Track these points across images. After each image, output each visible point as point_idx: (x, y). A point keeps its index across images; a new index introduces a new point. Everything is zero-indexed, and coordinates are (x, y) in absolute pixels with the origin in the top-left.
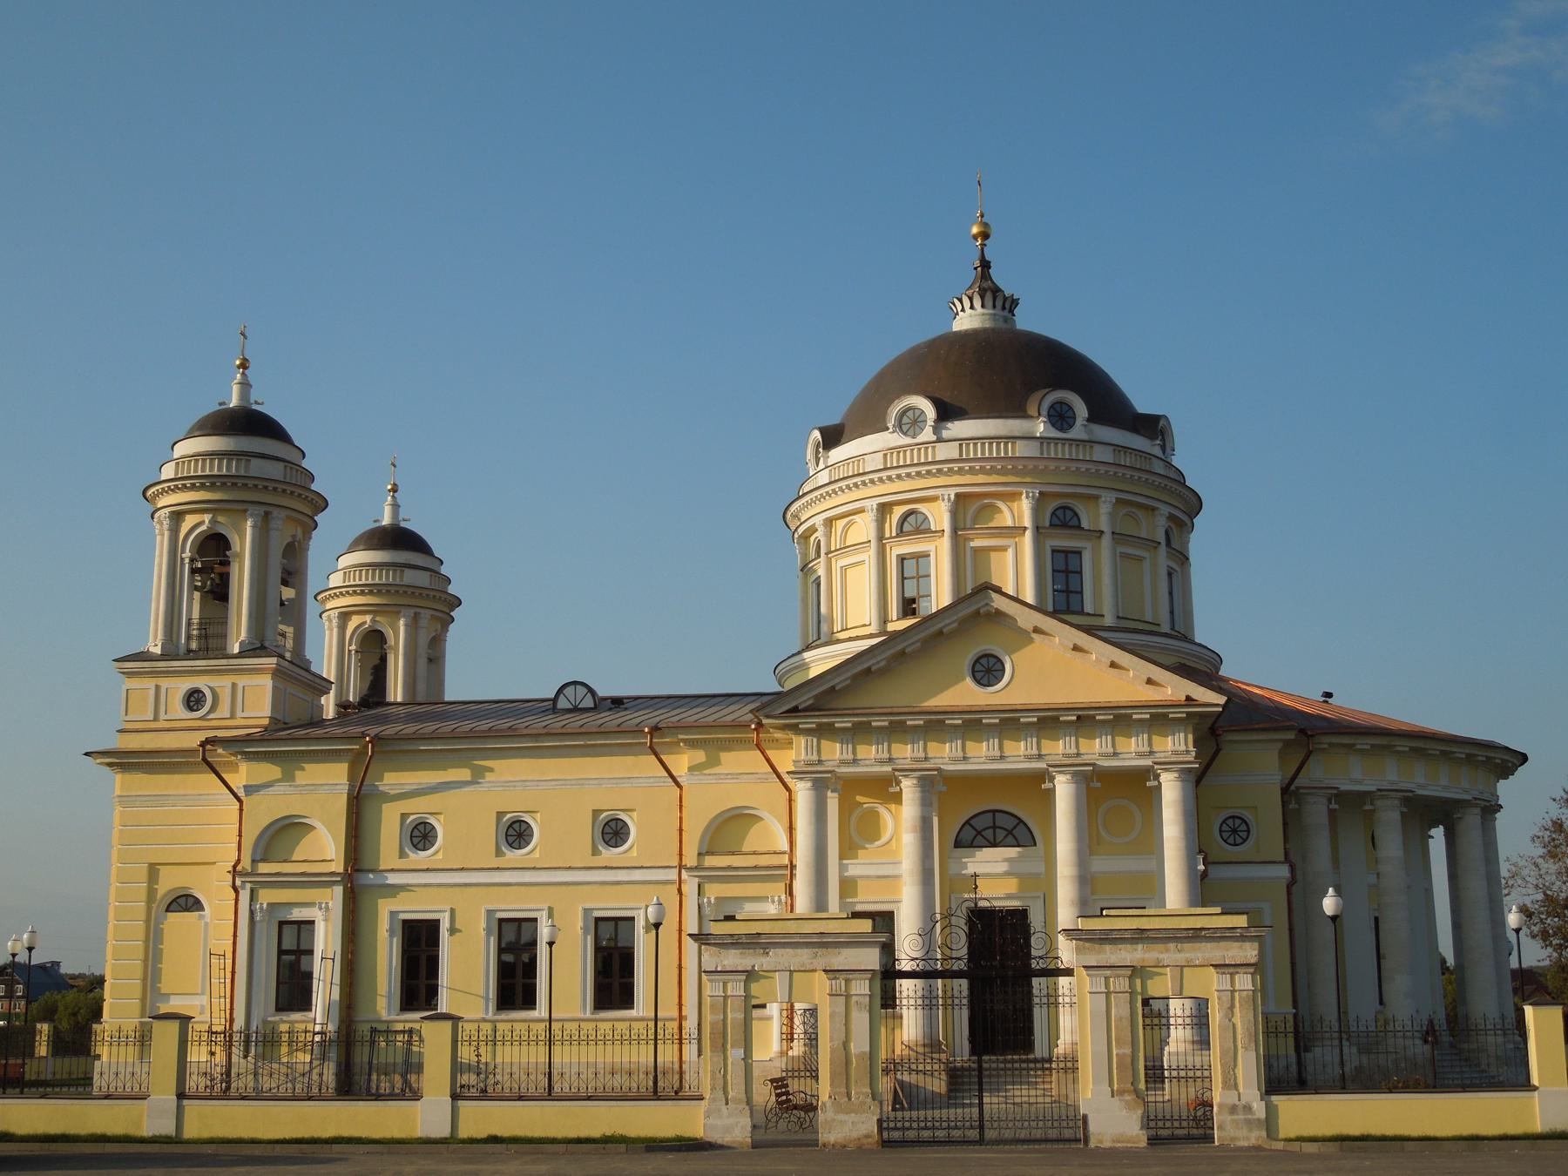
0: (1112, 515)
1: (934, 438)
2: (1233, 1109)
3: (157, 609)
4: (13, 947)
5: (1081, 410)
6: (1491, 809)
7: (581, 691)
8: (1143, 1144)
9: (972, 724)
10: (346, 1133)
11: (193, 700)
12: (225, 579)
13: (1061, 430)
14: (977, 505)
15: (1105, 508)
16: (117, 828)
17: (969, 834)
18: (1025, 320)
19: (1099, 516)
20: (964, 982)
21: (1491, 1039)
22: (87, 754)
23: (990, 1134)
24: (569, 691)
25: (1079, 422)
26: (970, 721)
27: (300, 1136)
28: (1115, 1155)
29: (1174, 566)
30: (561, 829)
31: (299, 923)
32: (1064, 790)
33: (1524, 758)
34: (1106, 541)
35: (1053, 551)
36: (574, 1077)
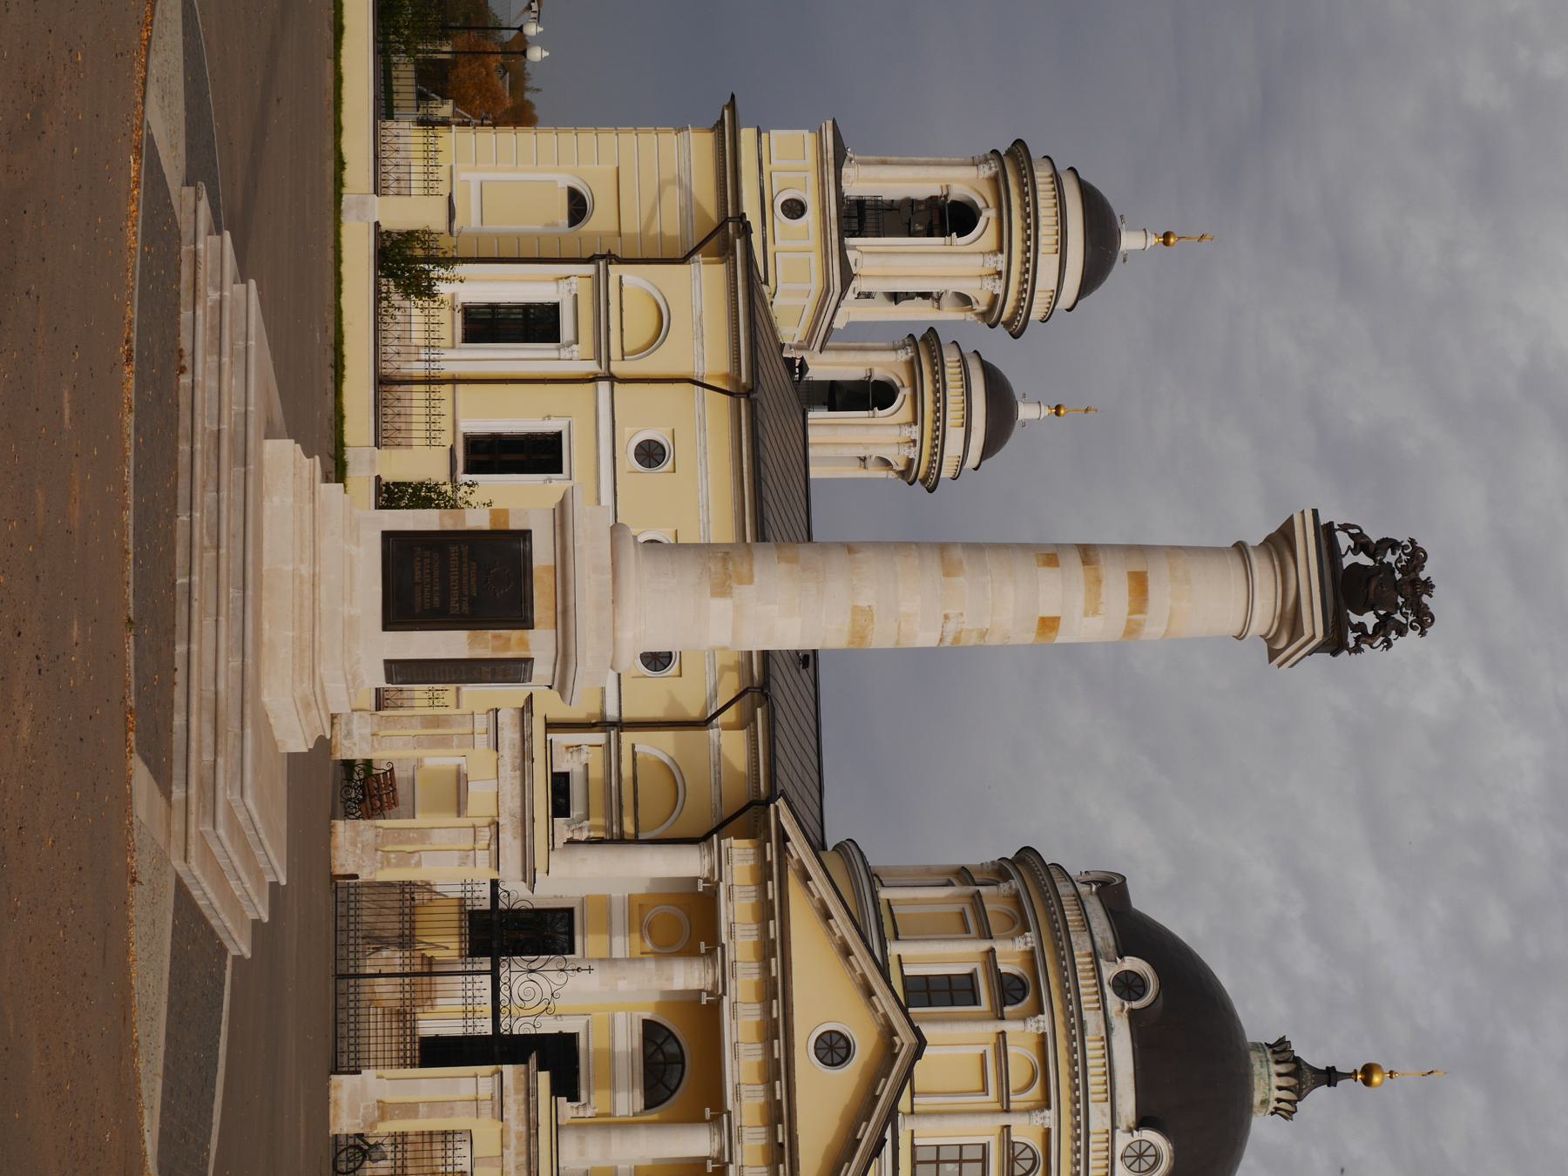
8: (334, 1130)
9: (776, 1029)
10: (345, 286)
11: (795, 209)
20: (486, 905)
22: (733, 96)
23: (342, 985)
26: (777, 1027)
28: (321, 1105)
32: (688, 976)
36: (395, 132)
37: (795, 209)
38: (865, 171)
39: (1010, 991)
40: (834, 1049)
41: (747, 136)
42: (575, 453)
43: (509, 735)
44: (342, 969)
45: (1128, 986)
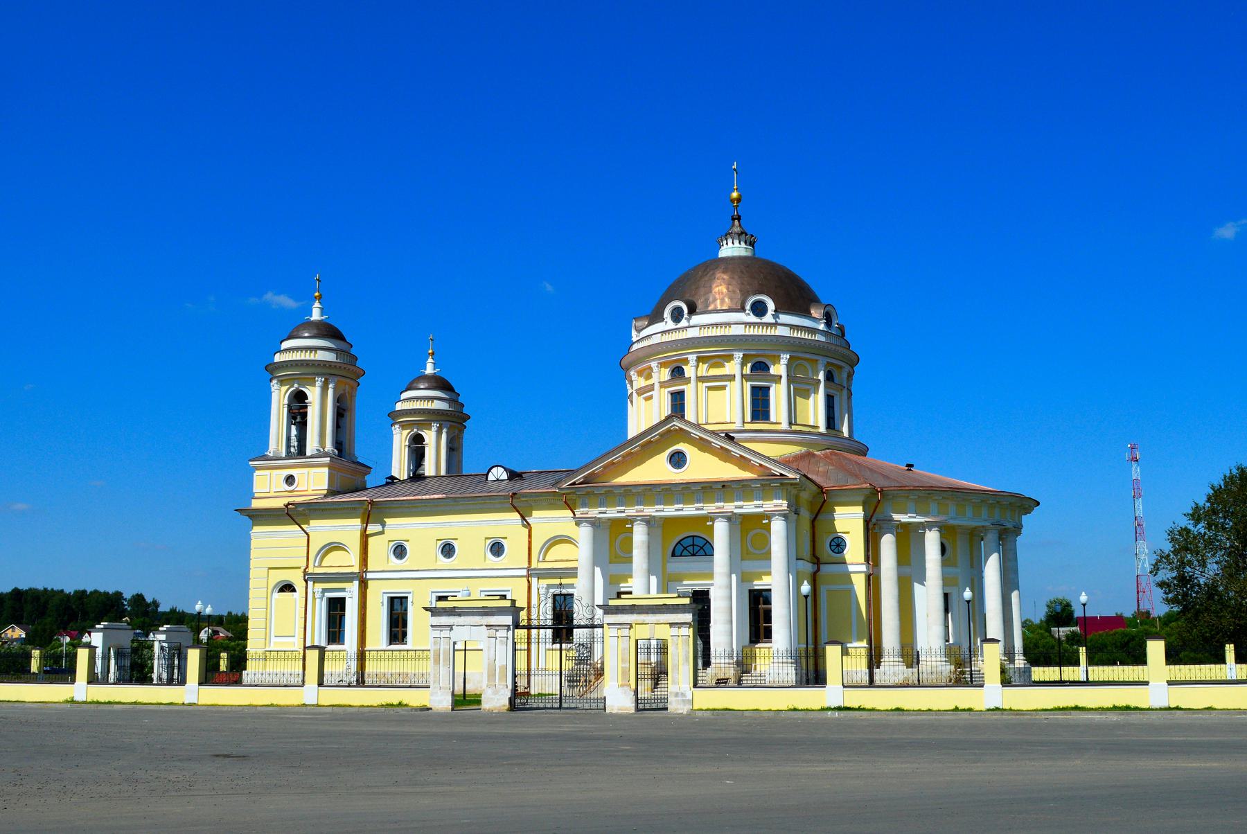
2: (677, 695)
3: (728, 324)
5: (771, 305)
7: (501, 470)
11: (290, 480)
12: (304, 415)
17: (680, 548)
19: (779, 369)
21: (68, 639)
24: (494, 470)
28: (620, 718)
30: (472, 550)
31: (401, 598)
32: (639, 534)
33: (1038, 504)
37: (290, 480)
38: (807, 417)
39: (678, 372)
40: (678, 460)
41: (256, 504)
42: (398, 589)
43: (444, 620)
44: (557, 705)
45: (677, 315)
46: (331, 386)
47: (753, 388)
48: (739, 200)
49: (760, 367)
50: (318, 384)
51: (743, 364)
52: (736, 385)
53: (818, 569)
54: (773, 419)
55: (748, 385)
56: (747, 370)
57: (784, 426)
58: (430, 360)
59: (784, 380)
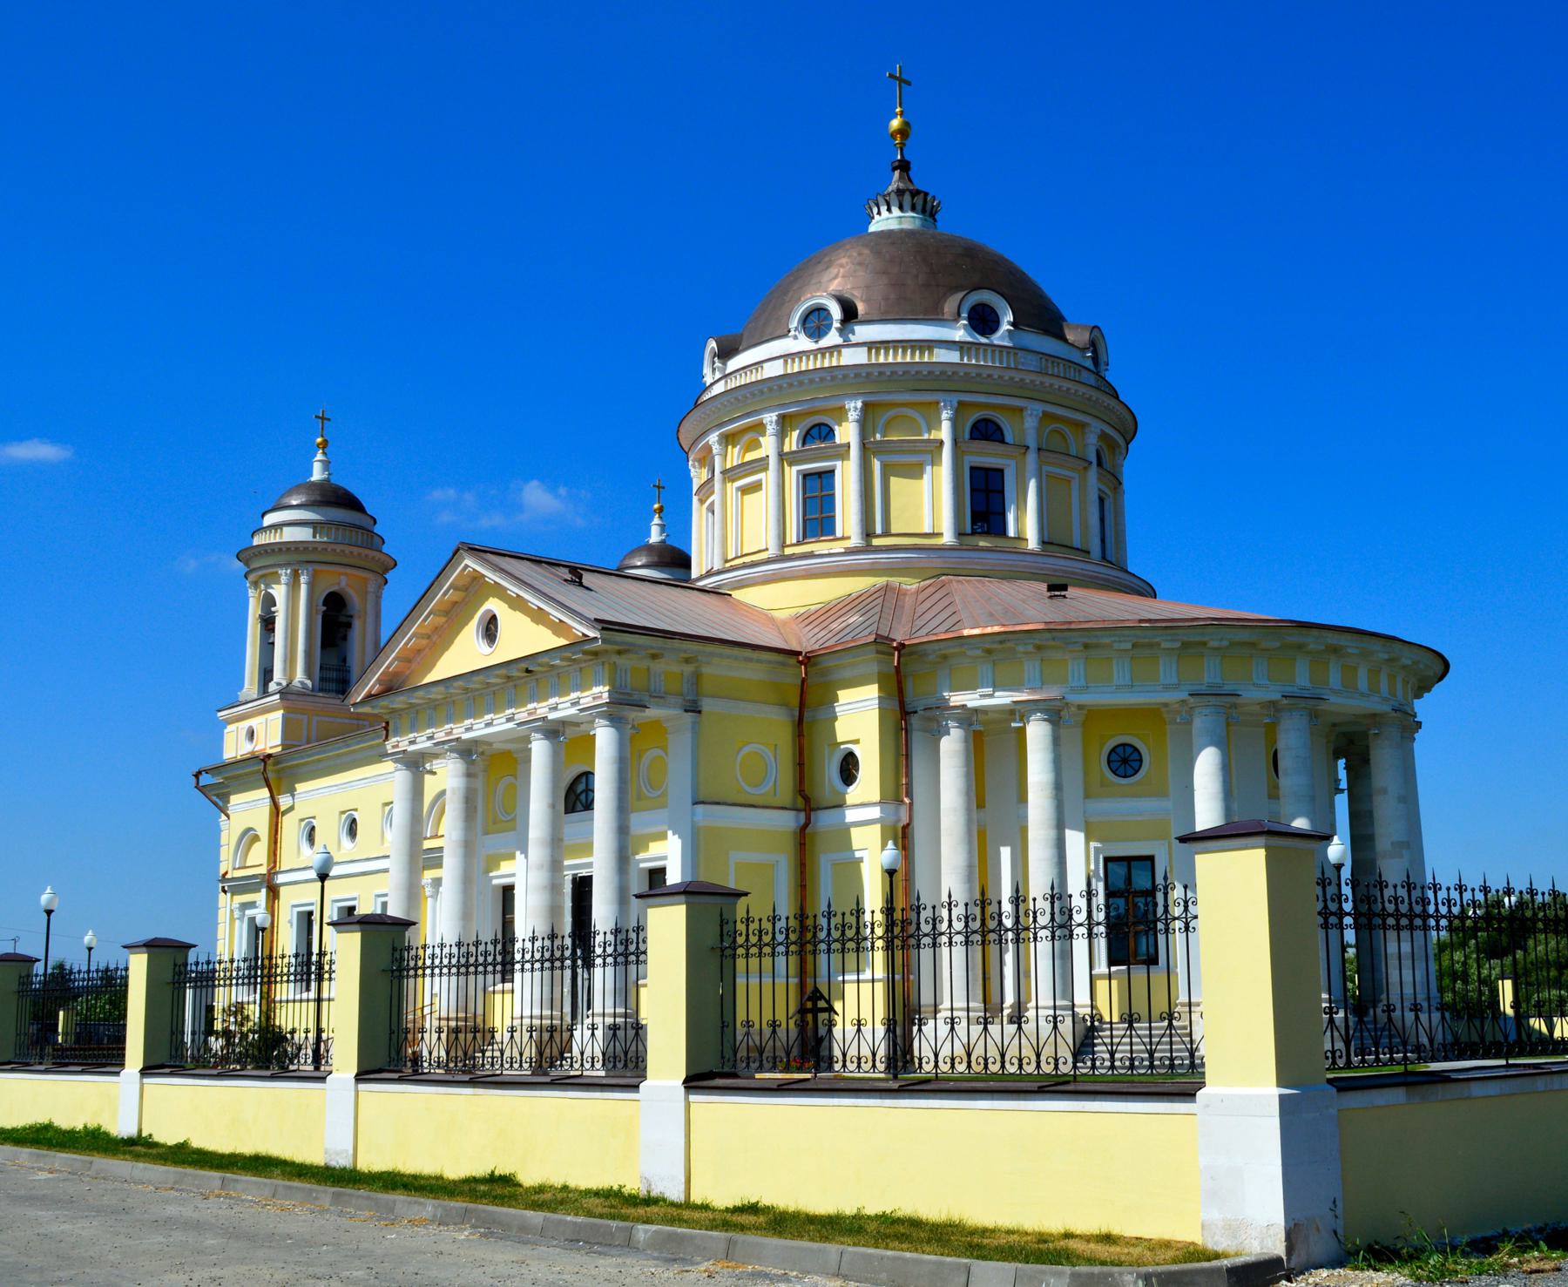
0: (1039, 431)
1: (839, 341)
4: (50, 901)
5: (1007, 318)
6: (1410, 726)
13: (983, 334)
14: (892, 412)
15: (1030, 423)
16: (779, 1076)
18: (951, 224)
19: (847, 433)
25: (1005, 327)
27: (848, 1207)
29: (1103, 488)
34: (1031, 458)
35: (972, 468)
40: (490, 630)
46: (303, 579)
47: (806, 476)
48: (904, 132)
49: (819, 433)
50: (284, 579)
51: (781, 435)
52: (769, 478)
53: (808, 819)
54: (839, 534)
55: (792, 473)
56: (792, 442)
57: (855, 540)
58: (656, 520)
59: (854, 452)
